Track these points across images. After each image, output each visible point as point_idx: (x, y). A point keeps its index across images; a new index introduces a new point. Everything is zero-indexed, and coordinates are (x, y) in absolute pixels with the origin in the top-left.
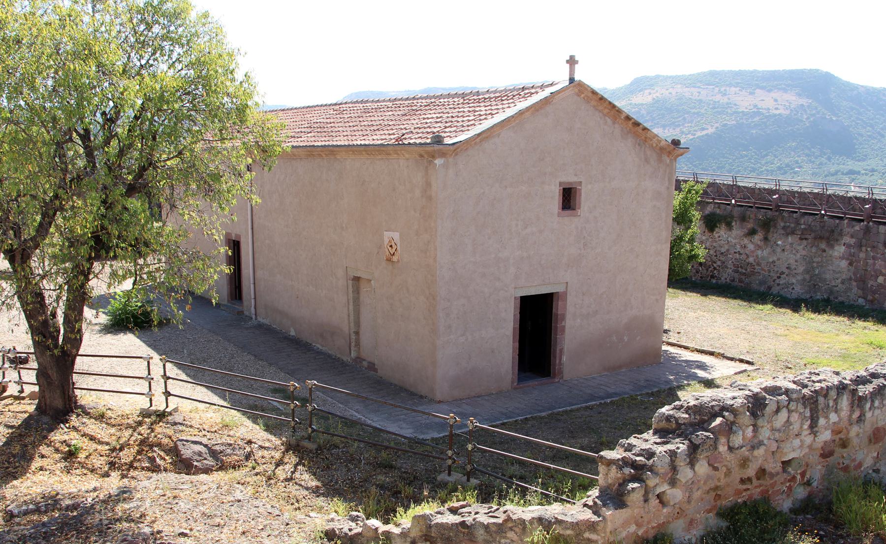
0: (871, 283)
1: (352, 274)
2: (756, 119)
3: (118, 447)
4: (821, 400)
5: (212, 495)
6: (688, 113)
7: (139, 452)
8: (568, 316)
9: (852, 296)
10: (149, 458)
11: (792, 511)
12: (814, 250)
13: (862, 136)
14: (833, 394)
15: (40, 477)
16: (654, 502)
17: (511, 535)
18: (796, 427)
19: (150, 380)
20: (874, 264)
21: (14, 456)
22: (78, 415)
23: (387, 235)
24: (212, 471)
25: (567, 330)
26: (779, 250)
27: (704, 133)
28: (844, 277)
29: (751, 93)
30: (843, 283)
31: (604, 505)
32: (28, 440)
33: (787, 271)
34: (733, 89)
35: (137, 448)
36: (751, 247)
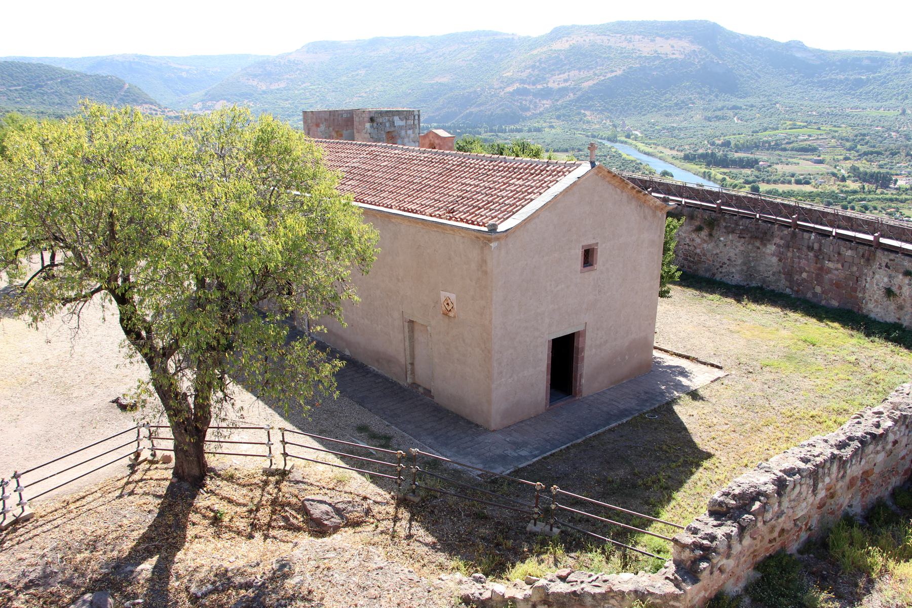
0: (796, 277)
1: (408, 318)
2: (657, 62)
3: (254, 508)
4: (820, 470)
5: (357, 563)
6: (600, 57)
7: (274, 512)
8: (587, 348)
9: (781, 286)
10: (283, 517)
11: (800, 552)
12: (750, 247)
13: (743, 76)
14: (828, 464)
15: (197, 546)
16: (716, 573)
17: (613, 601)
18: (804, 494)
19: (269, 444)
20: (799, 263)
21: (170, 527)
22: (211, 478)
23: (444, 295)
24: (339, 527)
25: (585, 360)
26: (721, 245)
27: (613, 74)
28: (774, 270)
29: (652, 41)
30: (773, 275)
31: (684, 581)
32: (178, 509)
33: (728, 262)
34: (637, 37)
35: (270, 508)
36: (698, 240)
